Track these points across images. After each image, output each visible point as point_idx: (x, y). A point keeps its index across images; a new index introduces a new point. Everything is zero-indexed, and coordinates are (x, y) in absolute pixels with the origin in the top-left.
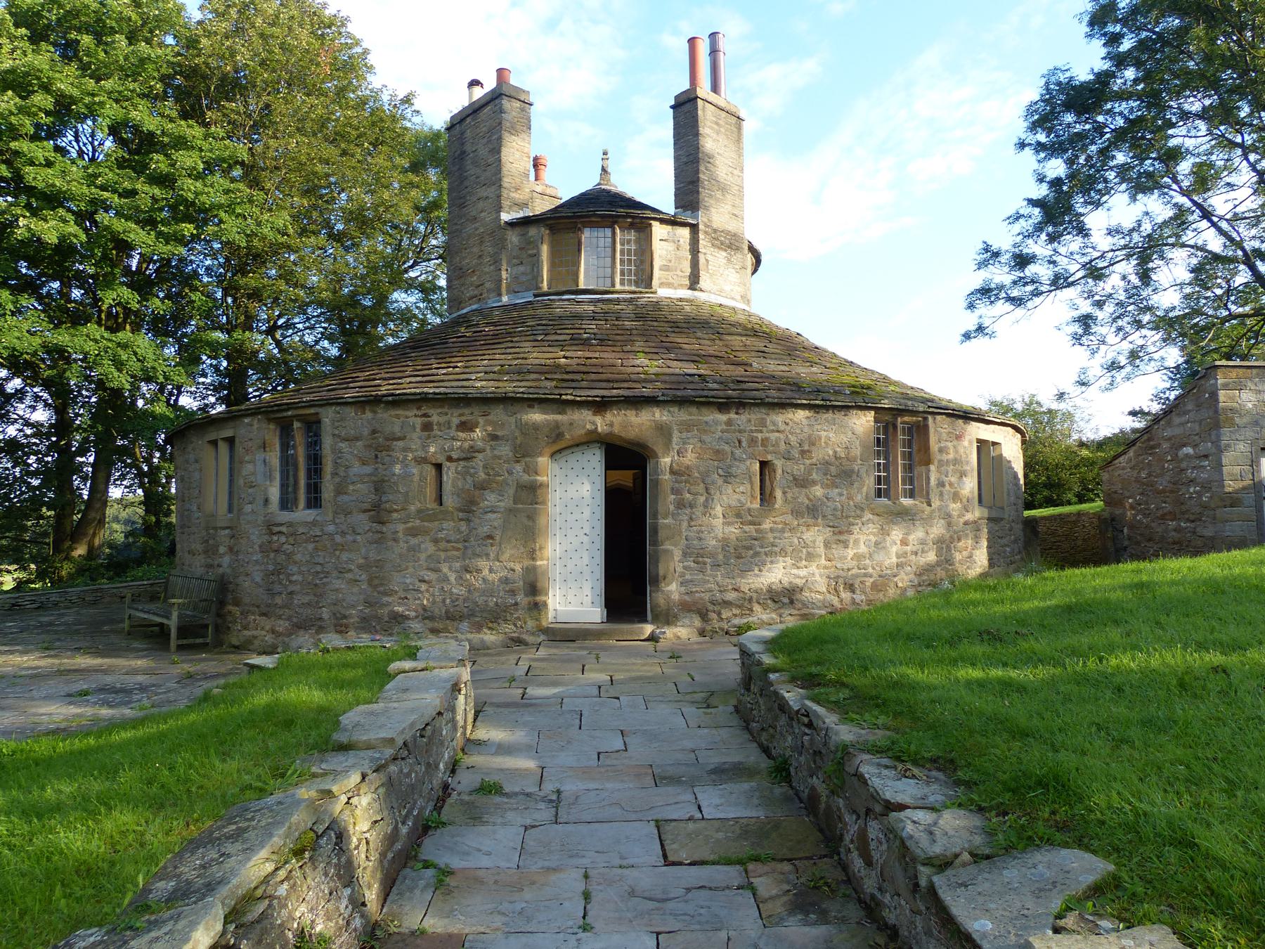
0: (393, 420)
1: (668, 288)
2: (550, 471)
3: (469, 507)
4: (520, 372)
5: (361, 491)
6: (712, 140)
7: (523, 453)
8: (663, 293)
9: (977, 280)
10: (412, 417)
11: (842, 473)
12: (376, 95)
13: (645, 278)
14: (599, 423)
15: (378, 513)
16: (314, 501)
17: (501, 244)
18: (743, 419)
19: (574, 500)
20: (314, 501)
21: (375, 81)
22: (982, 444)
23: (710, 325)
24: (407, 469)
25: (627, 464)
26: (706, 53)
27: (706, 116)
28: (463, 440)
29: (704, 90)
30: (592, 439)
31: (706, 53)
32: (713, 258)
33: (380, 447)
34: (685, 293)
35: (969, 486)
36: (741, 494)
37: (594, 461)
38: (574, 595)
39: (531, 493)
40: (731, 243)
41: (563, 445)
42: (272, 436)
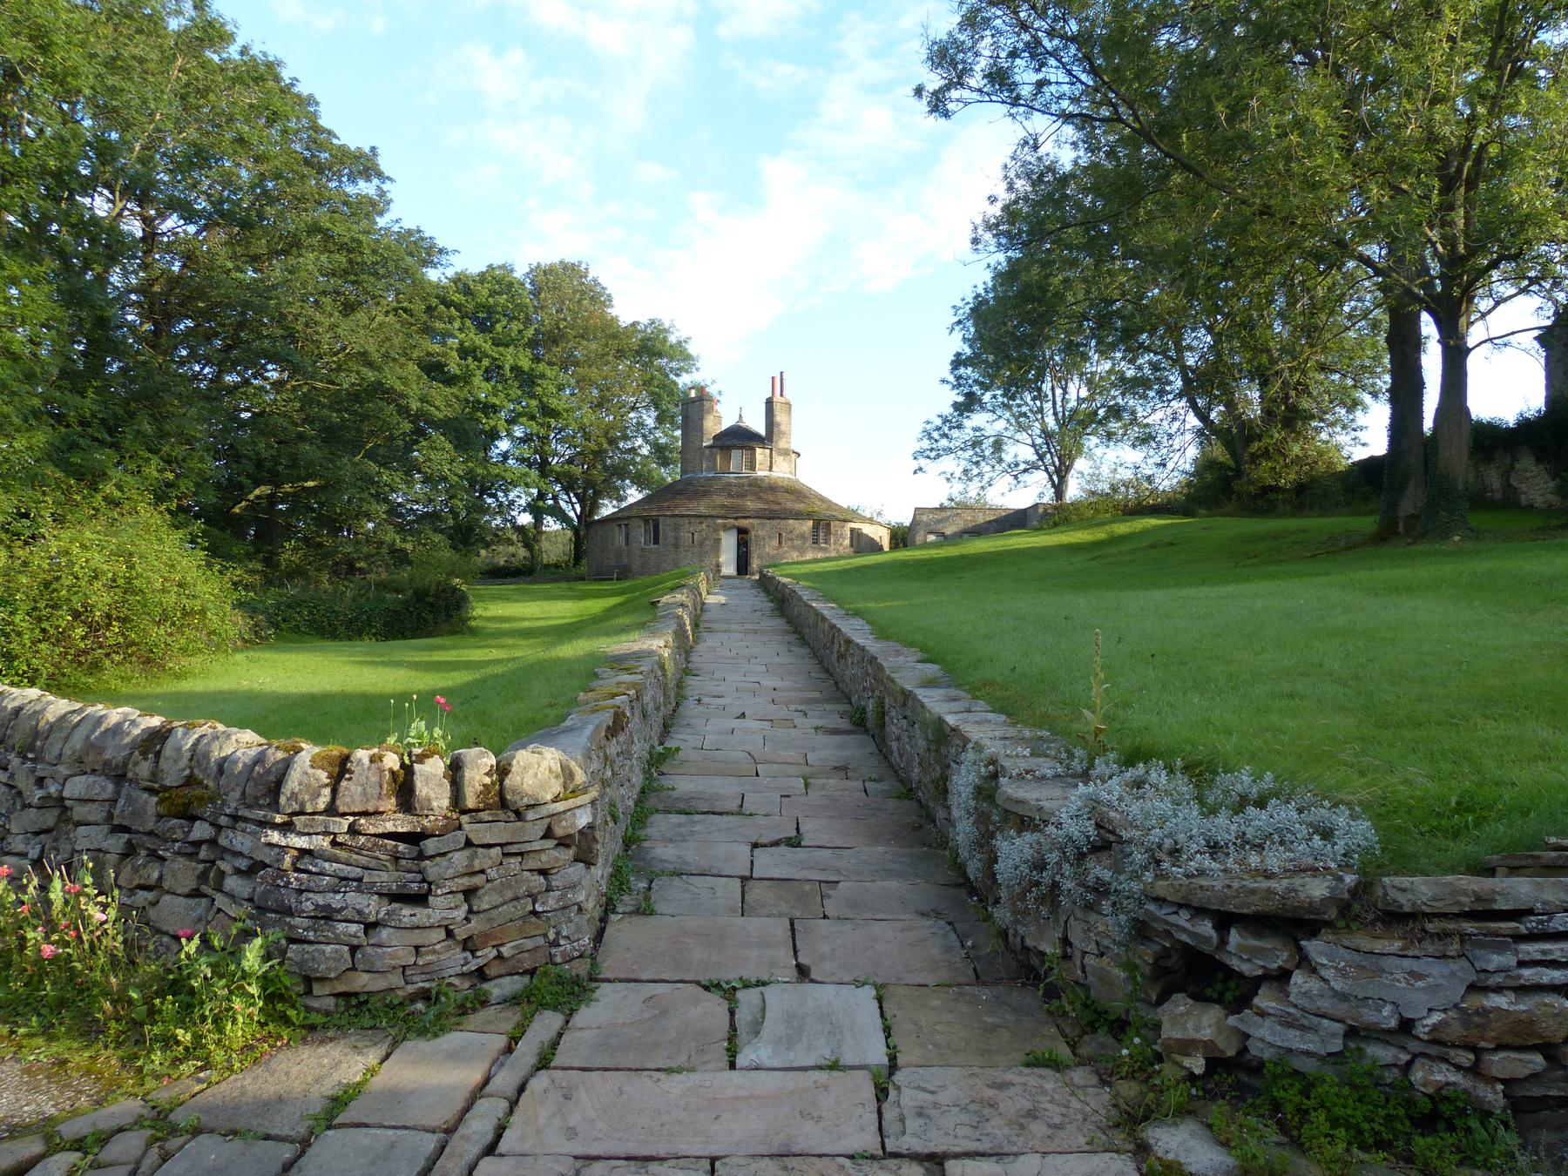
0: (680, 521)
1: (761, 473)
2: (723, 535)
3: (701, 544)
4: (714, 508)
5: (671, 540)
6: (779, 417)
7: (716, 531)
8: (760, 473)
9: (917, 447)
10: (686, 520)
11: (802, 536)
12: (614, 320)
13: (753, 468)
14: (737, 523)
15: (676, 546)
16: (656, 542)
17: (703, 454)
18: (775, 522)
19: (729, 542)
20: (656, 542)
21: (613, 312)
22: (852, 530)
23: (773, 487)
24: (685, 536)
25: (742, 532)
26: (778, 383)
27: (777, 408)
28: (699, 527)
29: (777, 398)
30: (734, 527)
31: (778, 383)
32: (778, 459)
33: (677, 528)
34: (767, 473)
35: (847, 542)
36: (775, 543)
37: (734, 533)
38: (729, 569)
39: (718, 540)
40: (786, 453)
41: (726, 528)
42: (641, 523)
